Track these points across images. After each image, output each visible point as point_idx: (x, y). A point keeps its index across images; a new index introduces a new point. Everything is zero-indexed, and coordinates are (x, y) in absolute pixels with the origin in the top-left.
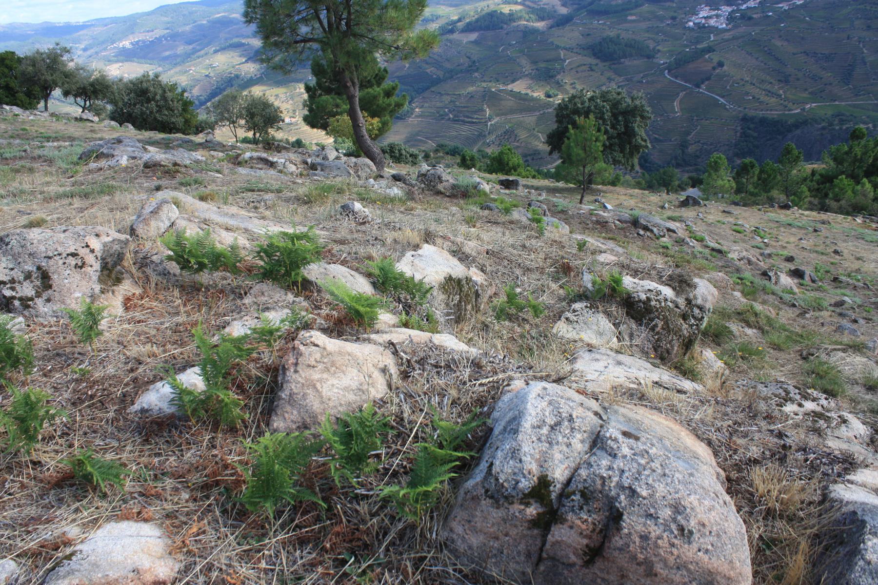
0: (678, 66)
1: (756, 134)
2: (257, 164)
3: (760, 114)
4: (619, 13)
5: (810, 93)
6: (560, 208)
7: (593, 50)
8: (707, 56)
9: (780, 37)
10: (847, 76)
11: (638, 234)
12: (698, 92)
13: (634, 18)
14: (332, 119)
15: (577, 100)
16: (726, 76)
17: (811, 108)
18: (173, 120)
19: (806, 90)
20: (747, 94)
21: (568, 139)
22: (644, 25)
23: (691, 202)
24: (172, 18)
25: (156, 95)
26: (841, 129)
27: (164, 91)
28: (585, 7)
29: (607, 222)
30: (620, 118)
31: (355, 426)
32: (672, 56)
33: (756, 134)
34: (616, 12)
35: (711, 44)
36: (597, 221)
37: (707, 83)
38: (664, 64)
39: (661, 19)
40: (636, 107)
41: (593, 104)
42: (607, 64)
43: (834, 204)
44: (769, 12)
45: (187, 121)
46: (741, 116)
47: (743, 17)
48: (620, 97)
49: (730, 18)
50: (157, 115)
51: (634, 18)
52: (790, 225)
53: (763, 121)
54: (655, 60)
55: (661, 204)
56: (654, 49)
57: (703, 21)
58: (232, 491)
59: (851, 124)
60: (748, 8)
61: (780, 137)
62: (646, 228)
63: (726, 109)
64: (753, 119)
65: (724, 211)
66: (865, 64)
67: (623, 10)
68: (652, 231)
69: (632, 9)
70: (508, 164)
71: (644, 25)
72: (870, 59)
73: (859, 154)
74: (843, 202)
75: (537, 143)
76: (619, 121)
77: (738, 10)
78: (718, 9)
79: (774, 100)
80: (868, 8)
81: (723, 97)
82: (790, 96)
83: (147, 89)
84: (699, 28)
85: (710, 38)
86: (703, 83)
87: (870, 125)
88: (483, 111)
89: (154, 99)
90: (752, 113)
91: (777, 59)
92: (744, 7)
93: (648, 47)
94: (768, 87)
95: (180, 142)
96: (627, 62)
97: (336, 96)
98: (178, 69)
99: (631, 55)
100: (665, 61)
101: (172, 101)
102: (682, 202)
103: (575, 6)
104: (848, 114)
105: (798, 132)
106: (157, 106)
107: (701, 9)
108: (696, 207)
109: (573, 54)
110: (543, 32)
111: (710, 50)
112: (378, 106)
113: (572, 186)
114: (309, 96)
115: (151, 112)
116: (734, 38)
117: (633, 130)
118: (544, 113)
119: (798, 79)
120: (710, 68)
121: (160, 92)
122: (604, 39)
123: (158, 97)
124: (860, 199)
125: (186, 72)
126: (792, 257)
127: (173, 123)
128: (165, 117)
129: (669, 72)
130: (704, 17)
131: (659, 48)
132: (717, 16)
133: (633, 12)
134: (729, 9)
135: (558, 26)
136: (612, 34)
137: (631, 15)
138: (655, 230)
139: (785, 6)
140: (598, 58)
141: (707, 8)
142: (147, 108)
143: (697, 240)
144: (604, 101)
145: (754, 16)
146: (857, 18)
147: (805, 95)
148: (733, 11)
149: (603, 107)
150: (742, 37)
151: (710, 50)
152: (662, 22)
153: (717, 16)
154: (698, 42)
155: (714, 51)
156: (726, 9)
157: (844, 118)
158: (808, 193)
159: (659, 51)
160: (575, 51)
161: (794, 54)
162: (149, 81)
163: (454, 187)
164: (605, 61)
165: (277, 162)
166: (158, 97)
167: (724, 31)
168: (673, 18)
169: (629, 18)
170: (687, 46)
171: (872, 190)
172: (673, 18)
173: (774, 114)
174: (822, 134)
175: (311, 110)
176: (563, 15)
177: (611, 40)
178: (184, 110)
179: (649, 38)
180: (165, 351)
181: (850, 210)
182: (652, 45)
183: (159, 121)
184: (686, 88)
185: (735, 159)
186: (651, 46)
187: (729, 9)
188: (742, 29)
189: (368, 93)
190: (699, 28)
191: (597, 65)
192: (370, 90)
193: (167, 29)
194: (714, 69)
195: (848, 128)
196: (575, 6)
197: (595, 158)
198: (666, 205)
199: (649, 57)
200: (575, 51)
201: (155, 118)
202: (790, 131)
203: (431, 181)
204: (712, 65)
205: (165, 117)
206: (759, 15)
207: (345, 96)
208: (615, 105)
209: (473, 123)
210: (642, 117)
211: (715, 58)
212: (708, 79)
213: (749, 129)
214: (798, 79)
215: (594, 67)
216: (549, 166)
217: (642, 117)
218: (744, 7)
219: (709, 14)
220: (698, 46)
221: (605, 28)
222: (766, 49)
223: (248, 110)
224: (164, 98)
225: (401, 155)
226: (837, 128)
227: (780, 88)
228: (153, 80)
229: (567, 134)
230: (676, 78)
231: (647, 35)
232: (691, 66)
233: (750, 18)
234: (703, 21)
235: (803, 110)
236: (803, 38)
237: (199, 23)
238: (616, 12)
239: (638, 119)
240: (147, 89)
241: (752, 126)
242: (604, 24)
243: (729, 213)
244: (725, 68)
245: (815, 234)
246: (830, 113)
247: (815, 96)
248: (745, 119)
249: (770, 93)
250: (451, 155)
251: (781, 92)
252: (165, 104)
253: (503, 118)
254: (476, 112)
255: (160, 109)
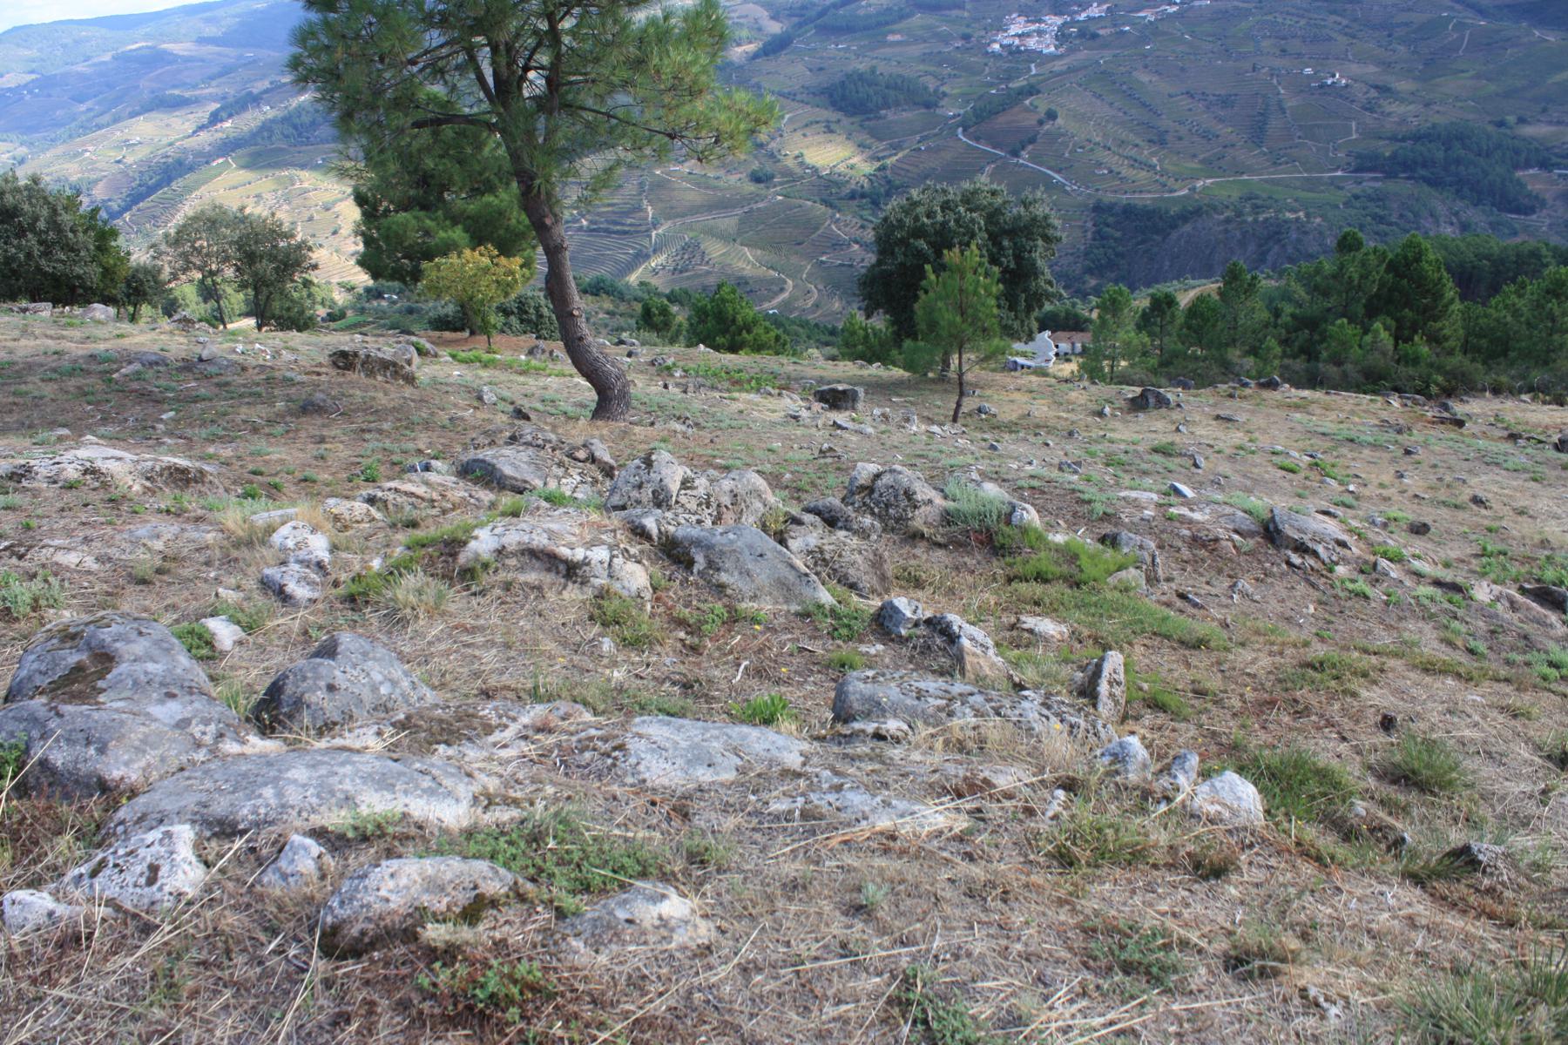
0: (981, 118)
1: (1118, 234)
2: (521, 569)
3: (1124, 198)
4: (874, 28)
5: (1201, 162)
6: (1099, 508)
7: (831, 96)
8: (1027, 102)
9: (1146, 67)
10: (1257, 133)
11: (1289, 563)
12: (1017, 164)
13: (897, 37)
14: (425, 265)
15: (920, 210)
16: (1062, 135)
17: (1205, 188)
18: (78, 270)
19: (1194, 156)
20: (1099, 165)
21: (926, 292)
22: (916, 50)
23: (1152, 400)
24: (40, 50)
25: (36, 219)
26: (1256, 220)
27: (54, 211)
28: (812, 20)
29: (1216, 540)
30: (1006, 243)
32: (968, 102)
33: (1118, 234)
34: (866, 28)
35: (1033, 81)
36: (1195, 539)
37: (1030, 147)
38: (954, 116)
39: (945, 39)
40: (1034, 219)
41: (951, 216)
42: (856, 119)
43: (1332, 370)
44: (1124, 24)
45: (107, 272)
46: (1091, 202)
47: (1082, 34)
48: (999, 200)
49: (1062, 36)
50: (43, 262)
51: (897, 37)
52: (1352, 441)
53: (1129, 212)
54: (939, 111)
55: (1097, 408)
56: (936, 91)
57: (1017, 42)
59: (1270, 214)
60: (1090, 19)
61: (1158, 238)
62: (1301, 548)
63: (1066, 192)
64: (1110, 208)
65: (1218, 417)
66: (1283, 111)
67: (879, 24)
68: (1315, 554)
69: (894, 22)
70: (734, 321)
71: (916, 50)
72: (1290, 103)
73: (1356, 276)
74: (1349, 367)
75: (741, 264)
76: (1002, 248)
77: (1074, 23)
78: (1040, 21)
79: (1143, 174)
80: (1280, 20)
81: (1059, 171)
82: (1170, 168)
83: (15, 208)
84: (1011, 53)
85: (1029, 69)
87: (1301, 214)
88: (639, 209)
89: (32, 227)
90: (1109, 198)
92: (1083, 16)
93: (926, 88)
94: (1133, 153)
95: (136, 366)
96: (890, 115)
97: (422, 214)
98: (60, 149)
99: (897, 103)
100: (957, 111)
101: (72, 230)
102: (1133, 400)
103: (796, 20)
104: (1264, 195)
105: (1187, 228)
106: (41, 243)
107: (1013, 22)
108: (1163, 411)
109: (795, 105)
110: (741, 67)
111: (1031, 91)
112: (507, 229)
113: (898, 373)
114: (364, 214)
115: (29, 255)
116: (1071, 70)
117: (1034, 264)
118: (751, 210)
119: (1180, 139)
120: (1034, 122)
121: (45, 212)
122: (848, 76)
123: (41, 225)
124: (1376, 360)
125: (77, 155)
126: (1425, 525)
127: (79, 277)
128: (60, 266)
129: (965, 130)
130: (1019, 36)
131: (944, 89)
132: (1040, 33)
133: (895, 27)
134: (1059, 21)
135: (766, 54)
136: (862, 66)
137: (893, 32)
138: (1320, 549)
139: (1148, 15)
140: (840, 109)
141: (1022, 19)
142: (19, 248)
143: (1391, 560)
144: (971, 210)
145: (1101, 32)
146: (1264, 37)
147: (1194, 165)
148: (1064, 24)
149: (973, 221)
150: (1086, 67)
151: (1031, 91)
152: (947, 43)
153: (1040, 33)
154: (1009, 79)
155: (1038, 92)
156: (1054, 22)
157: (1259, 202)
158: (1278, 350)
159: (944, 94)
160: (799, 97)
161: (1170, 96)
162: (17, 190)
163: (948, 518)
164: (853, 114)
165: (586, 562)
166: (41, 225)
167: (1053, 58)
168: (966, 37)
169: (891, 38)
170: (991, 85)
171: (1391, 341)
172: (966, 37)
173: (1146, 199)
174: (1226, 231)
175: (368, 241)
176: (774, 36)
177: (861, 77)
178: (98, 248)
179: (927, 73)
181: (1362, 379)
182: (932, 84)
183: (45, 274)
184: (995, 159)
185: (1087, 277)
186: (931, 88)
187: (1059, 21)
188: (1083, 55)
189: (489, 205)
190: (1011, 53)
191: (839, 121)
192: (488, 198)
193: (32, 72)
194: (1041, 123)
195: (1266, 219)
196: (796, 20)
197: (984, 330)
198: (1107, 410)
199: (928, 106)
200: (799, 97)
201: (39, 269)
202: (1174, 227)
203: (888, 506)
204: (1037, 117)
205: (60, 266)
206: (1108, 31)
207: (440, 213)
208: (993, 216)
209: (625, 233)
210: (1047, 239)
211: (1041, 104)
212: (1032, 141)
213: (1108, 225)
214: (1180, 139)
215: (833, 126)
216: (766, 305)
217: (1047, 239)
218: (1083, 16)
219: (1026, 30)
221: (846, 56)
223: (240, 245)
224: (54, 225)
225: (541, 316)
226: (1250, 219)
227: (1153, 154)
228: (27, 188)
229: (924, 283)
230: (977, 139)
231: (922, 67)
232: (1002, 120)
233: (1094, 36)
234: (1017, 42)
235: (1193, 189)
236: (1182, 69)
237: (96, 60)
238: (866, 28)
239: (1040, 242)
240: (15, 208)
241: (1111, 220)
242: (846, 50)
243: (1228, 420)
244: (1060, 121)
245: (1408, 459)
246: (1236, 195)
247: (1212, 166)
248: (1098, 208)
249: (1136, 163)
250: (592, 294)
251: (1155, 160)
252: (56, 237)
253: (679, 221)
254: (627, 214)
255: (47, 250)
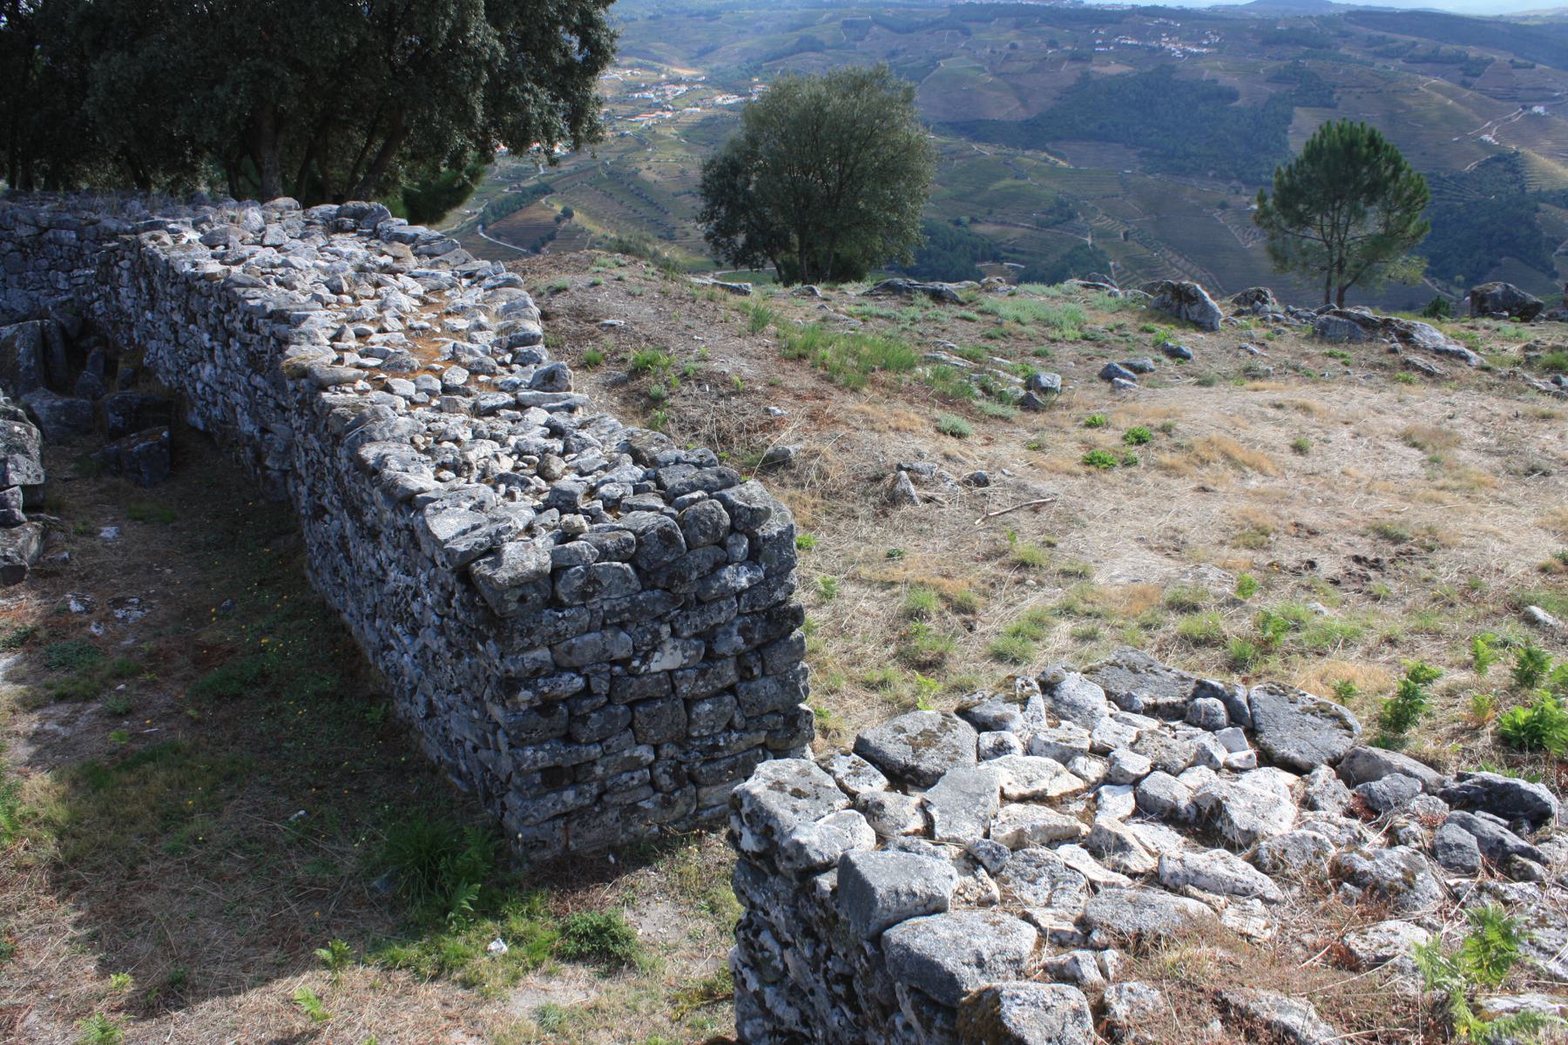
8: (543, 201)
31: (1409, 282)
35: (544, 180)
37: (550, 244)
38: (471, 214)
58: (572, 452)
86: (544, 244)
91: (651, 203)
129: (484, 228)
155: (552, 191)
180: (20, 607)
212: (551, 238)
220: (524, 184)
222: (632, 187)
230: (498, 237)
232: (520, 217)
